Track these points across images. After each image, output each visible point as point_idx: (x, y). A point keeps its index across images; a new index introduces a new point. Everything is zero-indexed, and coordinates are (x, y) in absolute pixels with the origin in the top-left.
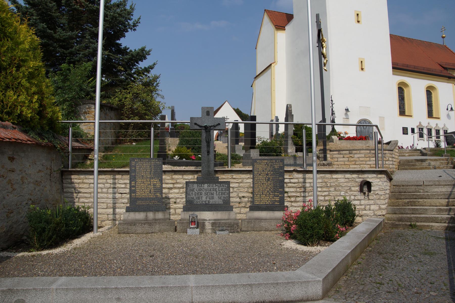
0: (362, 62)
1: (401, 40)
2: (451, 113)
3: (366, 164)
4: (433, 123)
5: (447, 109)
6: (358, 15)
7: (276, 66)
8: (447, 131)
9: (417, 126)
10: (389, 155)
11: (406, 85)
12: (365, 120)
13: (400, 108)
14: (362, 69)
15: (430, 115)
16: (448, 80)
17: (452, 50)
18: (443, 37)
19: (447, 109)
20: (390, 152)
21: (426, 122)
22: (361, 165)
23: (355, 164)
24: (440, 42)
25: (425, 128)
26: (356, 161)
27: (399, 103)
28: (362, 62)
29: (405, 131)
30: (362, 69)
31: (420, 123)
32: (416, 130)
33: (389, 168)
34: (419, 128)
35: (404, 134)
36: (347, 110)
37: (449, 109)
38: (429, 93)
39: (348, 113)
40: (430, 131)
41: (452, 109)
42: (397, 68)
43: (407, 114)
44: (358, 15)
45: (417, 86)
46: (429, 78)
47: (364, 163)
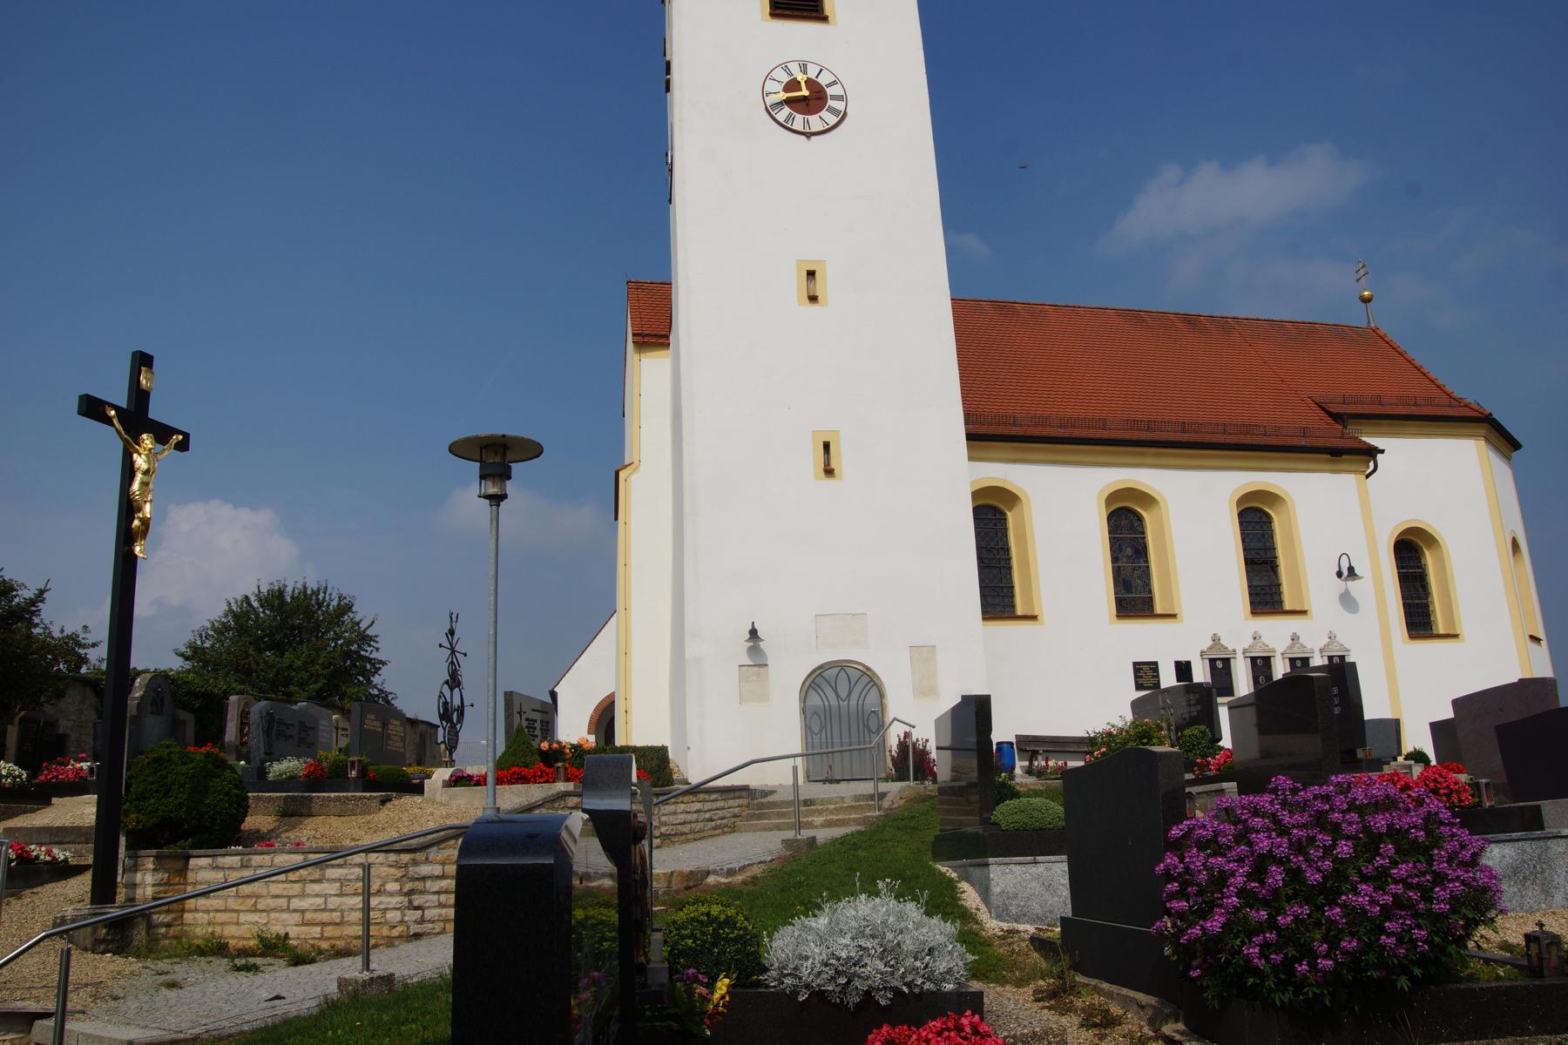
0: (827, 446)
1: (1180, 325)
2: (1353, 585)
3: (288, 910)
5: (1339, 574)
6: (811, 274)
7: (634, 478)
8: (1307, 659)
9: (1202, 653)
10: (385, 870)
11: (1148, 500)
12: (842, 666)
14: (829, 472)
16: (1334, 462)
18: (1366, 301)
20: (392, 857)
22: (273, 915)
23: (255, 910)
24: (1356, 317)
25: (1240, 656)
26: (258, 897)
28: (827, 446)
30: (829, 472)
31: (1216, 639)
33: (386, 923)
34: (1253, 659)
36: (753, 633)
37: (1345, 573)
38: (1256, 520)
41: (1351, 569)
42: (985, 434)
43: (1158, 609)
44: (811, 274)
46: (1127, 460)
47: (283, 902)
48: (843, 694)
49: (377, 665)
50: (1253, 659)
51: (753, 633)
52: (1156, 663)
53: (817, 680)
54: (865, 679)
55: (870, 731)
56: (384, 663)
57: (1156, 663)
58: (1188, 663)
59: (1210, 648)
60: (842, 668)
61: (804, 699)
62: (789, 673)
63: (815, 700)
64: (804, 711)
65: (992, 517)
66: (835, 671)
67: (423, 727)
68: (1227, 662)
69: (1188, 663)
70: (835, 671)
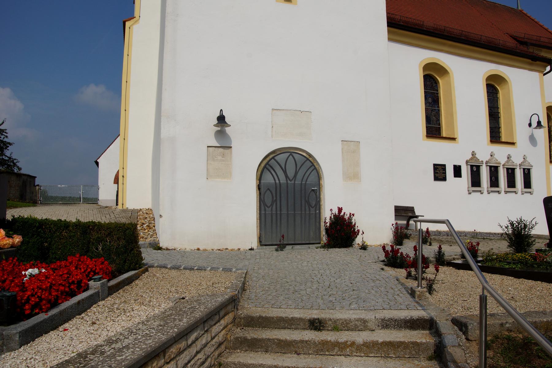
4: (501, 154)
5: (530, 125)
7: (135, 28)
9: (467, 162)
12: (291, 152)
13: (428, 119)
15: (495, 136)
17: (533, 17)
19: (530, 125)
21: (486, 151)
25: (484, 165)
27: (426, 110)
29: (439, 173)
31: (473, 154)
32: (465, 171)
35: (436, 179)
36: (221, 119)
37: (534, 124)
38: (493, 87)
39: (227, 129)
40: (494, 171)
43: (444, 134)
45: (467, 75)
48: (291, 174)
49: (6, 145)
50: (524, 169)
51: (221, 119)
52: (444, 165)
53: (268, 164)
54: (308, 164)
55: (310, 206)
56: (10, 144)
57: (444, 165)
58: (460, 167)
59: (471, 159)
60: (291, 154)
61: (260, 178)
62: (248, 156)
63: (268, 178)
64: (259, 187)
65: (432, 79)
66: (284, 156)
67: (25, 178)
68: (478, 167)
69: (460, 167)
70: (284, 156)
